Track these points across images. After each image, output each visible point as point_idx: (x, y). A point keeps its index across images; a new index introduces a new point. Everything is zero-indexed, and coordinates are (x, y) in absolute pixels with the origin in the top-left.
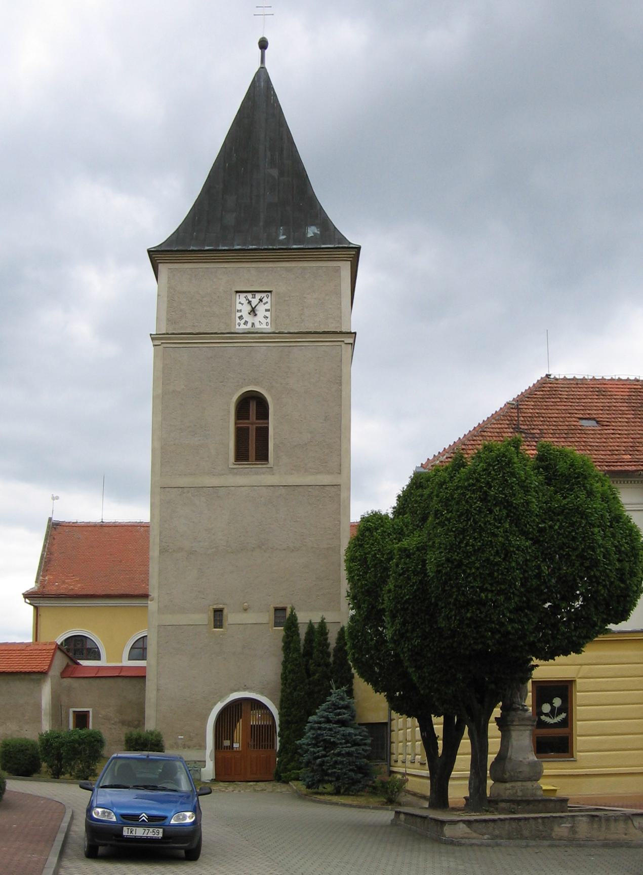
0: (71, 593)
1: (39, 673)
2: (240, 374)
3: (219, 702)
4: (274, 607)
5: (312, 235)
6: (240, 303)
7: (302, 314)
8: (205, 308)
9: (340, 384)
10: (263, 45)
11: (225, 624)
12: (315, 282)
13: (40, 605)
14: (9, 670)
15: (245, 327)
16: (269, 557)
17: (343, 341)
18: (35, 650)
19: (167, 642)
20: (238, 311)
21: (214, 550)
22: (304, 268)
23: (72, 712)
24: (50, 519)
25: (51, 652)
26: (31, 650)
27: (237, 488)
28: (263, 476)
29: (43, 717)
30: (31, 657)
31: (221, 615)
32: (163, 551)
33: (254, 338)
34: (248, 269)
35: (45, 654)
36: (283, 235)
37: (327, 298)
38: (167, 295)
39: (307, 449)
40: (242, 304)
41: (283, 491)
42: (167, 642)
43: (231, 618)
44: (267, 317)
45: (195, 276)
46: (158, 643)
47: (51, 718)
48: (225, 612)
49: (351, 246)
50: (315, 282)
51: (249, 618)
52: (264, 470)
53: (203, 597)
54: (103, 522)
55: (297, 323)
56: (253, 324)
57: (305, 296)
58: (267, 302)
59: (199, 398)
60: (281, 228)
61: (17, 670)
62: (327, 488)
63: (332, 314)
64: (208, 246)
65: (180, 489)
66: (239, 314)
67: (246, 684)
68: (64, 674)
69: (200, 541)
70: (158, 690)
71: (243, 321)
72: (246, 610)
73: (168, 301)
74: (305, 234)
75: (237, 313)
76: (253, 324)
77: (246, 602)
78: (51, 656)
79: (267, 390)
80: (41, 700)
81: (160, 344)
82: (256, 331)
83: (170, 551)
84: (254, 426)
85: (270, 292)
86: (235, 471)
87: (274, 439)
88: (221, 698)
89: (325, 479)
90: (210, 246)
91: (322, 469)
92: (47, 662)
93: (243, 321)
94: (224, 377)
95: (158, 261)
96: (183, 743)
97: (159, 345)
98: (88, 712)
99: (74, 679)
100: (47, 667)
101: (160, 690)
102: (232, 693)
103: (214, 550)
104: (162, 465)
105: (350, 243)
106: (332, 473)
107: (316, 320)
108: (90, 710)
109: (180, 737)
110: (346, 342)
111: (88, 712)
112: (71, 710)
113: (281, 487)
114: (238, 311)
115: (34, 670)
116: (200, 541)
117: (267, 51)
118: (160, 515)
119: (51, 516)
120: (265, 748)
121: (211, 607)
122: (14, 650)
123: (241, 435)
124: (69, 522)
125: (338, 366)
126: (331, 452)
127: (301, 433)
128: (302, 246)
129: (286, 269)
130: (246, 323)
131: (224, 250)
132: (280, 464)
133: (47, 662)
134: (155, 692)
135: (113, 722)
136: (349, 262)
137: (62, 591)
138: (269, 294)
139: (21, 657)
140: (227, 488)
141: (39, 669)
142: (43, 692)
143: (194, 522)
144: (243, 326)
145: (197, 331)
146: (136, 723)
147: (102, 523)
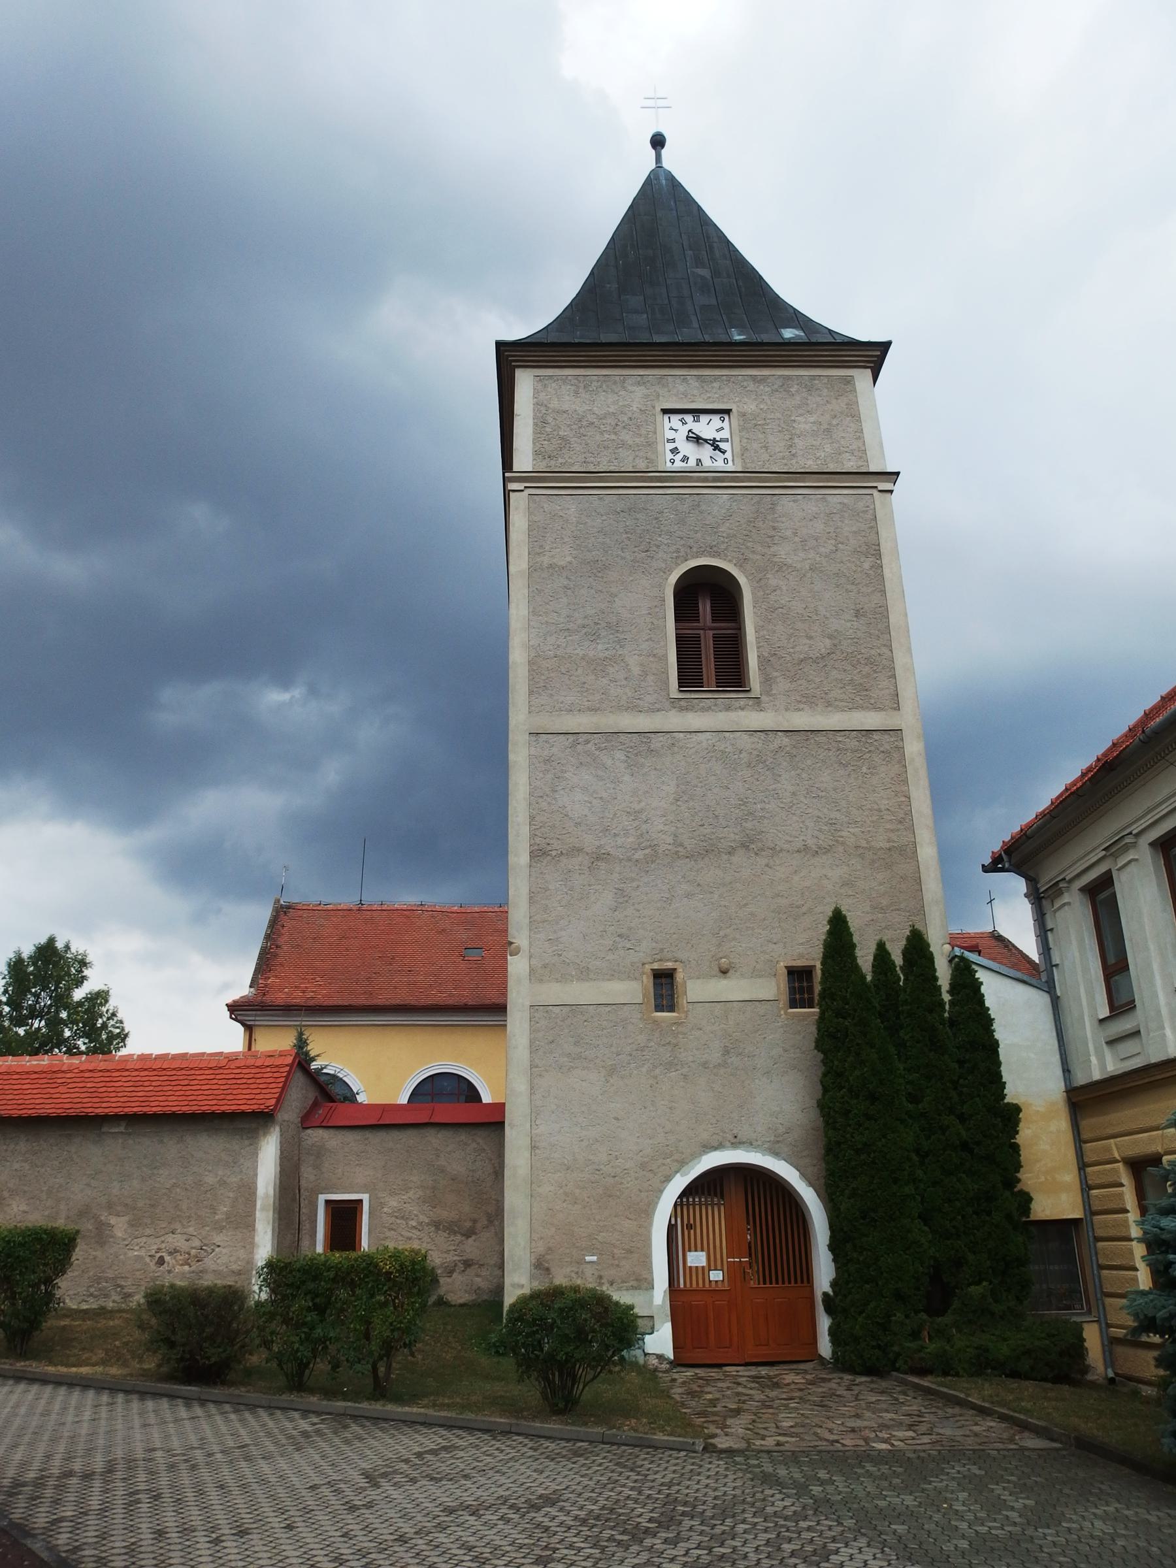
0: (311, 1003)
2: (682, 538)
3: (678, 1175)
6: (671, 429)
7: (791, 446)
9: (878, 555)
10: (658, 142)
11: (682, 1002)
13: (257, 1023)
14: (184, 1109)
15: (684, 464)
16: (767, 865)
17: (876, 487)
18: (248, 1067)
20: (668, 441)
22: (789, 378)
23: (323, 1202)
25: (282, 1070)
26: (239, 1068)
27: (688, 736)
28: (741, 713)
29: (258, 1214)
30: (239, 1081)
32: (538, 854)
34: (682, 377)
35: (271, 1075)
37: (834, 422)
40: (676, 429)
41: (785, 740)
47: (276, 1216)
48: (679, 976)
51: (733, 989)
52: (742, 702)
53: (628, 946)
55: (783, 459)
56: (699, 461)
58: (722, 429)
59: (602, 577)
62: (876, 736)
63: (848, 447)
66: (671, 446)
68: (307, 1121)
69: (615, 835)
70: (533, 1148)
72: (724, 972)
75: (667, 444)
78: (283, 1079)
79: (735, 565)
80: (256, 1175)
81: (523, 488)
83: (554, 853)
84: (711, 633)
85: (728, 412)
86: (683, 703)
87: (758, 648)
88: (682, 1164)
89: (870, 720)
92: (273, 1091)
93: (678, 457)
96: (596, 1274)
97: (522, 491)
98: (361, 1201)
99: (332, 1131)
100: (273, 1101)
101: (538, 1148)
102: (705, 1153)
104: (531, 693)
106: (881, 709)
107: (818, 454)
108: (322, 1198)
109: (588, 1258)
110: (879, 489)
111: (361, 1201)
112: (322, 1198)
113: (780, 733)
114: (668, 441)
115: (242, 1107)
117: (664, 152)
118: (530, 785)
121: (648, 967)
122: (201, 1069)
123: (687, 648)
125: (871, 527)
126: (875, 672)
127: (810, 638)
129: (754, 378)
133: (273, 1091)
134: (527, 1154)
135: (414, 1223)
136: (869, 370)
139: (216, 1081)
140: (668, 735)
141: (255, 1107)
142: (261, 1156)
143: (601, 798)
144: (679, 465)
146: (468, 1224)
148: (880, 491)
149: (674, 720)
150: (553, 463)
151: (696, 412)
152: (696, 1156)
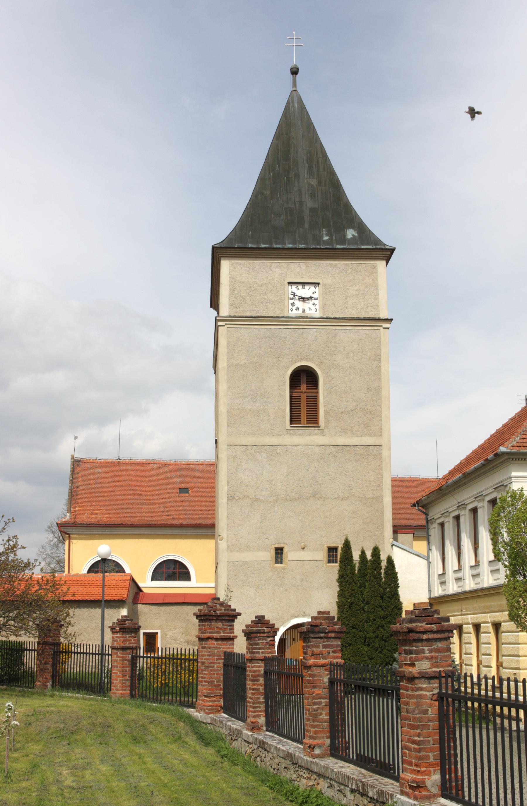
1: (119, 601)
2: (294, 351)
3: (282, 627)
4: (327, 547)
5: (351, 237)
7: (345, 303)
8: (262, 296)
9: (379, 361)
10: (295, 72)
12: (356, 276)
15: (296, 312)
16: (322, 504)
17: (382, 326)
19: (236, 576)
21: (274, 498)
24: (73, 457)
27: (293, 447)
28: (316, 437)
31: (282, 553)
32: (231, 498)
33: (306, 322)
36: (327, 236)
37: (366, 290)
38: (228, 284)
39: (353, 415)
41: (333, 449)
42: (236, 576)
43: (289, 555)
44: (316, 305)
45: (253, 269)
46: (228, 575)
48: (285, 550)
49: (387, 247)
50: (356, 276)
52: (316, 432)
54: (120, 459)
56: (304, 310)
57: (347, 287)
58: (315, 292)
60: (324, 230)
61: (98, 598)
62: (371, 448)
64: (263, 244)
65: (244, 446)
67: (304, 611)
71: (295, 307)
72: (303, 549)
73: (230, 289)
74: (345, 236)
76: (304, 310)
77: (303, 543)
81: (224, 325)
82: (306, 316)
83: (237, 498)
85: (318, 284)
86: (291, 432)
87: (324, 406)
90: (265, 244)
91: (366, 432)
93: (295, 307)
94: (280, 353)
95: (220, 255)
97: (224, 326)
100: (126, 596)
103: (274, 498)
104: (228, 426)
105: (385, 245)
106: (375, 435)
107: (358, 307)
108: (159, 631)
111: (157, 633)
116: (262, 491)
119: (73, 454)
120: (516, 681)
121: (273, 546)
124: (90, 460)
126: (373, 418)
128: (345, 247)
130: (297, 309)
131: (279, 248)
132: (330, 427)
137: (93, 521)
138: (317, 285)
143: (256, 474)
145: (256, 315)
147: (119, 460)
148: (384, 328)
149: (288, 440)
150: (238, 310)
151: (304, 284)
152: (289, 620)
